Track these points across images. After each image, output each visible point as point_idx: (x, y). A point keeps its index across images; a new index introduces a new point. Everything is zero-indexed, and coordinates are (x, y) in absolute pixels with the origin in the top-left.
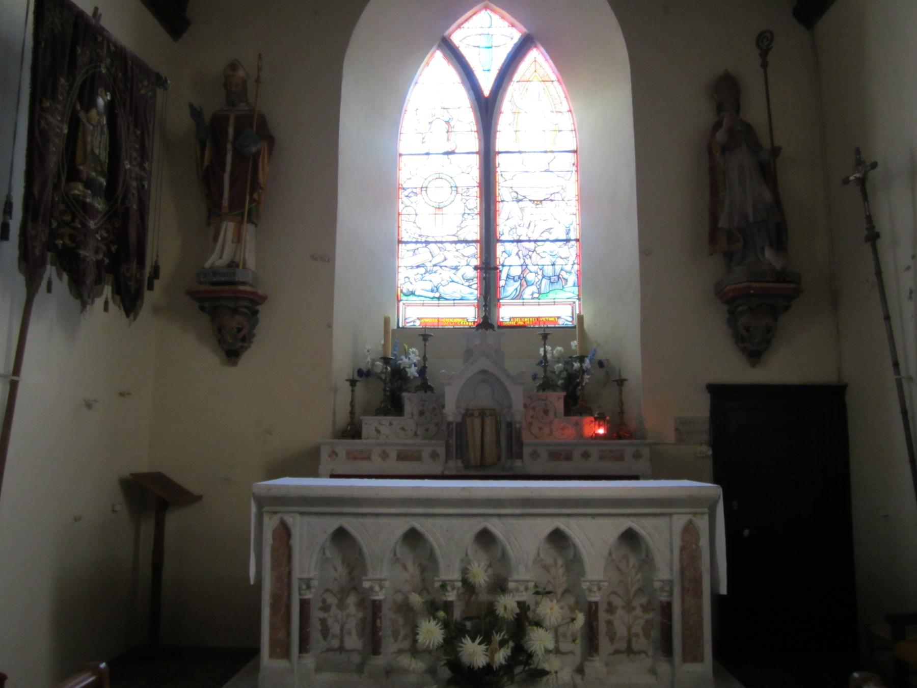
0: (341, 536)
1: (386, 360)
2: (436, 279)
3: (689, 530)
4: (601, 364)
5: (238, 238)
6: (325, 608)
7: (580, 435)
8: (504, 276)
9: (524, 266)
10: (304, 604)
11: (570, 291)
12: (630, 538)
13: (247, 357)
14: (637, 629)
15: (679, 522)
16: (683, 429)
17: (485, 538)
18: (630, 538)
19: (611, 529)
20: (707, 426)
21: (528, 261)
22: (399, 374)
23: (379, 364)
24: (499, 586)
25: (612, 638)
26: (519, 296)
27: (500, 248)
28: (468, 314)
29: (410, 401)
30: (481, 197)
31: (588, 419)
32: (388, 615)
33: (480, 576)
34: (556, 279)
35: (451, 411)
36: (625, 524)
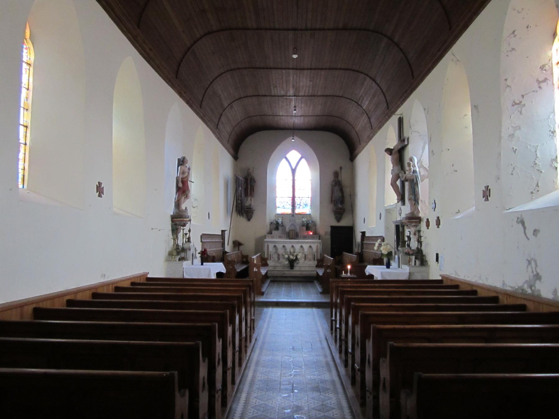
0: (275, 246)
1: (276, 221)
2: (283, 204)
3: (317, 246)
4: (313, 222)
5: (251, 200)
6: (273, 255)
7: (308, 234)
8: (296, 204)
9: (300, 202)
10: (270, 254)
11: (309, 207)
12: (310, 247)
13: (252, 220)
14: (311, 257)
15: (316, 245)
16: (326, 233)
17: (293, 246)
18: (310, 247)
19: (308, 245)
20: (330, 233)
21: (301, 201)
22: (277, 223)
23: (274, 222)
24: (294, 252)
25: (308, 259)
26: (299, 208)
27: (296, 199)
28: (289, 211)
29: (280, 228)
30: (292, 210)
31: (309, 231)
32: (280, 256)
33: (292, 251)
34: (306, 205)
35: (287, 230)
36: (310, 245)
